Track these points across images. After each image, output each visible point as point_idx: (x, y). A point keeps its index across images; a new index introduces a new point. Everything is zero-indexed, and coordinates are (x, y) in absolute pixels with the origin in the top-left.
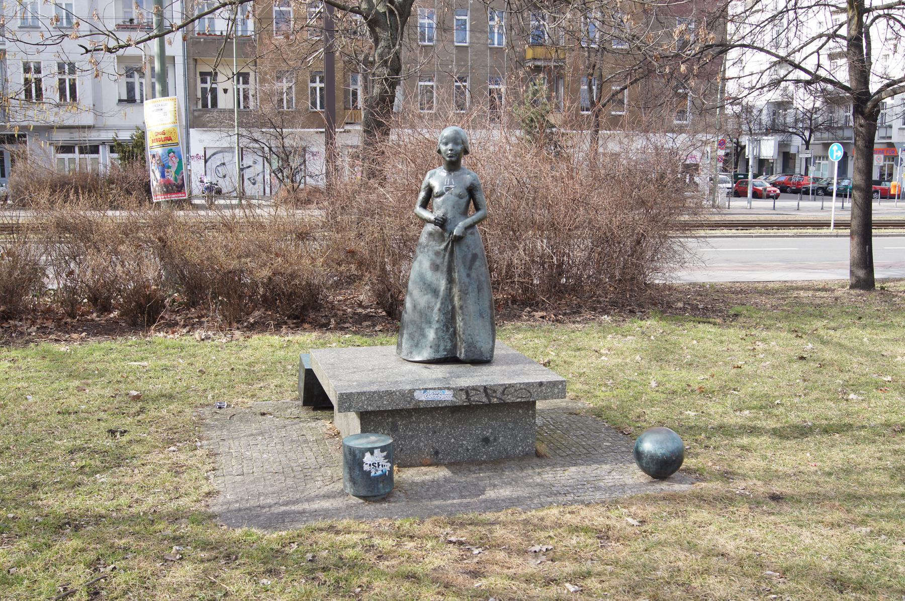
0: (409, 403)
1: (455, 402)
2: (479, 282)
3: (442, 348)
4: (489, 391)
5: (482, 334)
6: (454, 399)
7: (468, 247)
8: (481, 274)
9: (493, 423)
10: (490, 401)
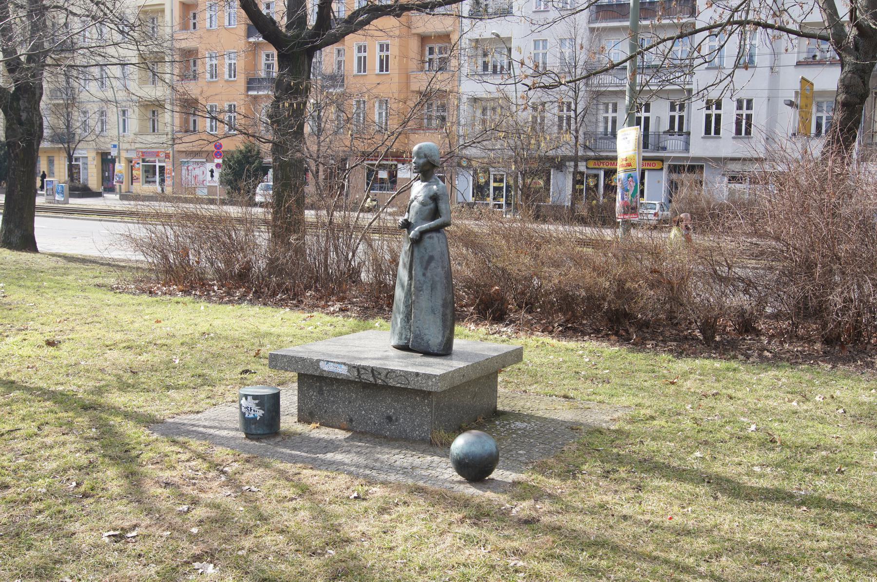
0: (316, 370)
1: (349, 377)
2: (433, 281)
3: (404, 336)
4: (375, 372)
5: (431, 329)
6: (349, 374)
7: (426, 249)
8: (436, 275)
9: (395, 404)
10: (376, 381)
